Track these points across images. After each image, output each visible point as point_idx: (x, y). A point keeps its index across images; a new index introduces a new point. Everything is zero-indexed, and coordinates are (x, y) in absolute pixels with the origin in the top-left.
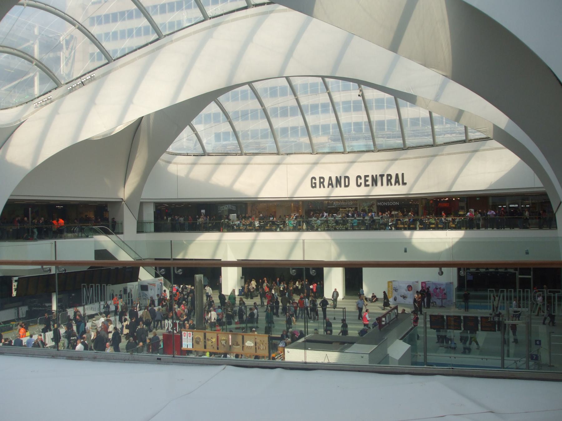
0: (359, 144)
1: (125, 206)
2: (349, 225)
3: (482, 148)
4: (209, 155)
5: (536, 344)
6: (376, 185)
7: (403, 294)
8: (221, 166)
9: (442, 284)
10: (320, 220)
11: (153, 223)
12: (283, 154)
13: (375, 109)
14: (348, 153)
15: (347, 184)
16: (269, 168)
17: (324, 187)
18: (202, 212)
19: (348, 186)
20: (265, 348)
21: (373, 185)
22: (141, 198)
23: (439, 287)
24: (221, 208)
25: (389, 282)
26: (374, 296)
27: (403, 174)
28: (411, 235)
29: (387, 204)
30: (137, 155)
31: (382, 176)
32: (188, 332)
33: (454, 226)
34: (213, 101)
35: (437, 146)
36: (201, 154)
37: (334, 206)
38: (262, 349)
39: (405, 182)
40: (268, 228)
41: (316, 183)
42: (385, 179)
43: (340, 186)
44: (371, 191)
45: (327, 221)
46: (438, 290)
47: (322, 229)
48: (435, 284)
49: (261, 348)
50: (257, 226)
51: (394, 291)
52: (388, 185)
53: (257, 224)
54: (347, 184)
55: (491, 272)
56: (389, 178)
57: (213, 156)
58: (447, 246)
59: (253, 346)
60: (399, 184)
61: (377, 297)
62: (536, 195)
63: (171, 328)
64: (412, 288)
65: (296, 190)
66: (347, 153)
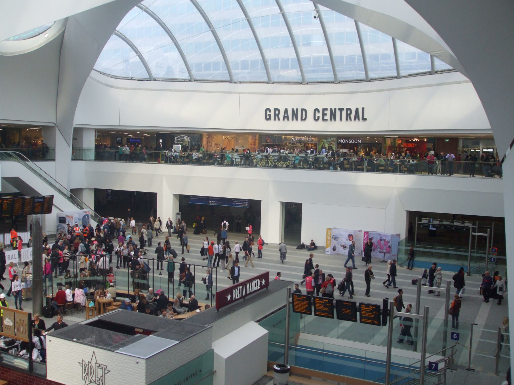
4: (155, 80)
5: (452, 338)
6: (335, 119)
7: (343, 244)
9: (387, 236)
10: (261, 155)
11: (94, 151)
12: (236, 82)
15: (304, 118)
17: (279, 119)
20: (24, 331)
21: (331, 120)
23: (383, 238)
25: (328, 229)
26: (313, 244)
27: (363, 109)
29: (348, 142)
31: (341, 110)
35: (401, 77)
36: (147, 79)
38: (21, 331)
40: (205, 161)
42: (344, 113)
43: (297, 119)
46: (383, 242)
47: (261, 166)
48: (380, 235)
49: (21, 330)
50: (195, 159)
51: (334, 239)
52: (347, 119)
54: (304, 118)
55: (445, 225)
56: (349, 113)
57: (160, 81)
59: (13, 326)
60: (359, 120)
61: (316, 245)
66: (306, 83)
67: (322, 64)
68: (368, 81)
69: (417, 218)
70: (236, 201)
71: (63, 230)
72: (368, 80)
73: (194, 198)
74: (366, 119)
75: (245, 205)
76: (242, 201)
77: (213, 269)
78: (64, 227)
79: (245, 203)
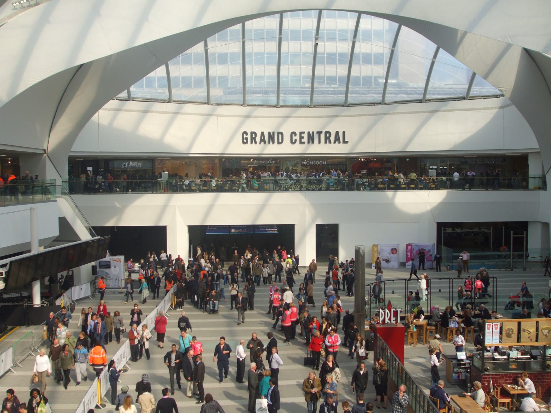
0: (295, 99)
1: (47, 160)
2: (323, 185)
6: (313, 142)
7: (385, 258)
8: (149, 115)
9: (428, 246)
12: (212, 104)
15: (280, 141)
16: (200, 119)
18: (88, 170)
19: (281, 143)
21: (309, 143)
24: (123, 165)
27: (344, 132)
28: (394, 196)
30: (77, 94)
31: (319, 133)
32: (494, 324)
33: (433, 186)
34: (398, 24)
35: (386, 104)
37: (255, 164)
39: (346, 140)
40: (227, 188)
42: (323, 137)
44: (307, 148)
52: (326, 142)
53: (214, 184)
54: (280, 141)
56: (328, 136)
58: (429, 208)
60: (339, 142)
62: (471, 157)
63: (388, 320)
64: (396, 250)
65: (227, 146)
68: (347, 106)
69: (491, 227)
72: (347, 105)
73: (212, 228)
74: (347, 142)
78: (108, 273)
79: (274, 229)
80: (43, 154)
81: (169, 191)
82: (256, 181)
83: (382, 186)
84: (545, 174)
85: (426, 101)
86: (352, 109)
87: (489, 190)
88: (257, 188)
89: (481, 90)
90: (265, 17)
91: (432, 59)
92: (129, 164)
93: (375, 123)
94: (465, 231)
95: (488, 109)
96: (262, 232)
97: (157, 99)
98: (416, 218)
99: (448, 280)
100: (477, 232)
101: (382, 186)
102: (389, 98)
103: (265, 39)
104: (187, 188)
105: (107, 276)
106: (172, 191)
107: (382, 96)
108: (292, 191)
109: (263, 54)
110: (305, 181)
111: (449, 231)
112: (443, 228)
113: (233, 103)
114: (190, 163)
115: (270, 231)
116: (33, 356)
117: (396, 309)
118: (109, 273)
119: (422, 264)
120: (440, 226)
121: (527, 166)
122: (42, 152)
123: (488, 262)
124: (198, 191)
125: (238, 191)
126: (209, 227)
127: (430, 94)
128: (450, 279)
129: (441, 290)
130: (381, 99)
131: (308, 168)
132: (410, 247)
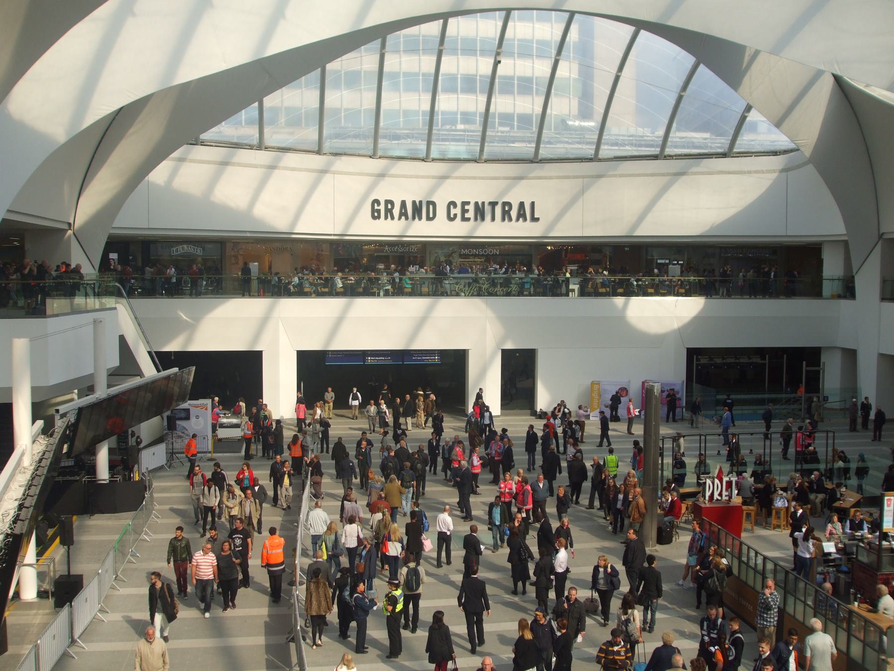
0: (456, 149)
3: (694, 169)
6: (483, 219)
8: (230, 169)
13: (499, 93)
14: (432, 160)
15: (431, 216)
19: (432, 219)
21: (476, 219)
22: (114, 226)
24: (173, 251)
27: (533, 204)
28: (626, 305)
30: (132, 130)
31: (493, 204)
35: (600, 160)
41: (380, 210)
42: (498, 210)
44: (475, 229)
45: (476, 280)
52: (503, 219)
54: (431, 216)
57: (212, 146)
58: (676, 325)
60: (525, 220)
64: (627, 391)
67: (401, 126)
68: (537, 162)
70: (418, 354)
71: (181, 434)
72: (538, 160)
73: (334, 354)
74: (537, 220)
75: (435, 359)
76: (428, 354)
77: (829, 434)
78: (185, 428)
79: (435, 356)
80: (67, 230)
81: (267, 294)
82: (407, 280)
83: (604, 290)
84: (854, 274)
85: (665, 157)
86: (548, 166)
87: (733, 299)
88: (410, 290)
89: (558, 136)
90: (459, 17)
91: (678, 92)
92: (183, 248)
93: (583, 191)
94: (728, 361)
95: (763, 172)
96: (415, 361)
97: (240, 143)
98: (657, 341)
99: (698, 438)
100: (747, 363)
101: (604, 290)
102: (606, 151)
103: (421, 51)
104: (296, 289)
105: (183, 433)
106: (271, 294)
107: (594, 147)
108: (465, 296)
109: (417, 74)
110: (485, 281)
111: (704, 361)
112: (695, 356)
113: (357, 152)
114: (282, 249)
115: (427, 359)
116: (134, 563)
117: (730, 479)
118: (187, 428)
119: (671, 414)
120: (692, 353)
121: (820, 263)
122: (66, 227)
123: (742, 410)
124: (313, 295)
125: (379, 295)
126: (330, 353)
127: (671, 146)
128: (700, 435)
129: (721, 452)
130: (593, 152)
131: (483, 260)
132: (596, 387)
